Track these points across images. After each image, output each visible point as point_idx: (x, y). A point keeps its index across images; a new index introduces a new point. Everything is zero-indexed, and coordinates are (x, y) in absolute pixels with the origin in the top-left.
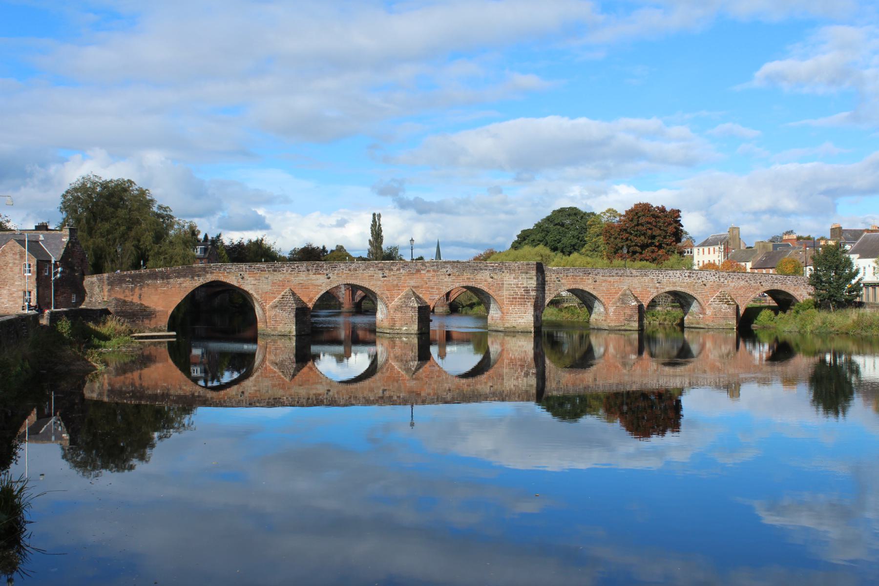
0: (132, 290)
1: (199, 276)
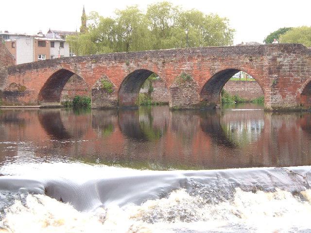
1: (53, 66)
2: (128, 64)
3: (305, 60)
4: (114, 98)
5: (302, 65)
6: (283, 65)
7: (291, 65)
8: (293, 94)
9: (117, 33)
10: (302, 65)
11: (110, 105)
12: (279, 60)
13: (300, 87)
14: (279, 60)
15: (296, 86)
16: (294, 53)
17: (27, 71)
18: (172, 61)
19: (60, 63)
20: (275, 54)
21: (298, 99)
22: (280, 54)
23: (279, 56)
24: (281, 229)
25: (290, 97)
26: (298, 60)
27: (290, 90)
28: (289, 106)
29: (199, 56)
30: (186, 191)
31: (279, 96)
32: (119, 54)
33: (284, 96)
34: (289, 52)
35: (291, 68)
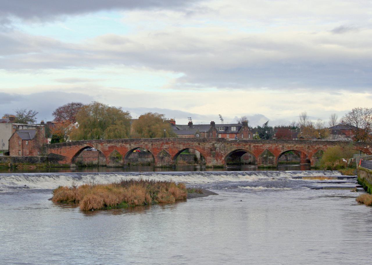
0: (58, 150)
2: (130, 145)
3: (225, 145)
4: (122, 162)
5: (224, 147)
6: (217, 147)
7: (220, 147)
8: (221, 160)
9: (163, 123)
10: (224, 147)
11: (120, 165)
12: (215, 145)
13: (223, 157)
14: (215, 145)
15: (222, 156)
16: (221, 142)
17: (64, 147)
18: (157, 144)
19: (86, 143)
20: (214, 142)
21: (222, 162)
22: (216, 143)
23: (216, 143)
24: (162, 115)
25: (219, 161)
26: (223, 145)
27: (219, 158)
28: (219, 165)
29: (172, 142)
30: (166, 119)
31: (215, 161)
32: (125, 140)
33: (217, 161)
34: (219, 142)
35: (220, 149)
